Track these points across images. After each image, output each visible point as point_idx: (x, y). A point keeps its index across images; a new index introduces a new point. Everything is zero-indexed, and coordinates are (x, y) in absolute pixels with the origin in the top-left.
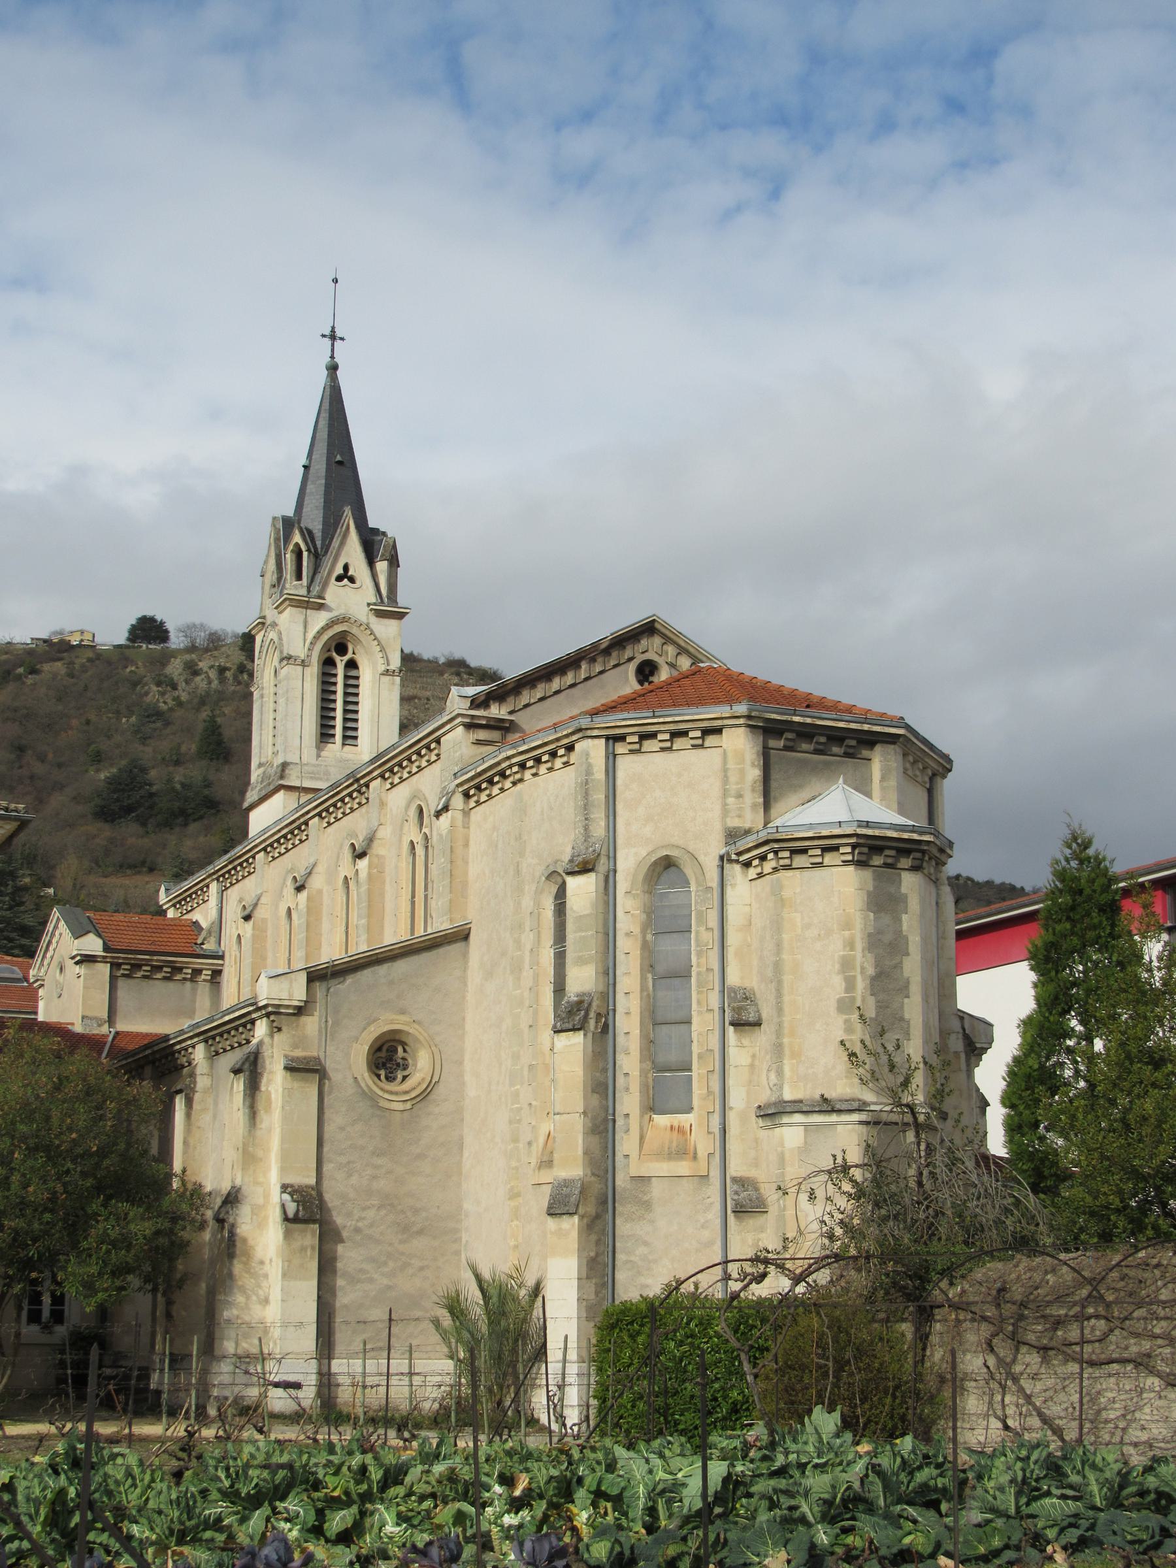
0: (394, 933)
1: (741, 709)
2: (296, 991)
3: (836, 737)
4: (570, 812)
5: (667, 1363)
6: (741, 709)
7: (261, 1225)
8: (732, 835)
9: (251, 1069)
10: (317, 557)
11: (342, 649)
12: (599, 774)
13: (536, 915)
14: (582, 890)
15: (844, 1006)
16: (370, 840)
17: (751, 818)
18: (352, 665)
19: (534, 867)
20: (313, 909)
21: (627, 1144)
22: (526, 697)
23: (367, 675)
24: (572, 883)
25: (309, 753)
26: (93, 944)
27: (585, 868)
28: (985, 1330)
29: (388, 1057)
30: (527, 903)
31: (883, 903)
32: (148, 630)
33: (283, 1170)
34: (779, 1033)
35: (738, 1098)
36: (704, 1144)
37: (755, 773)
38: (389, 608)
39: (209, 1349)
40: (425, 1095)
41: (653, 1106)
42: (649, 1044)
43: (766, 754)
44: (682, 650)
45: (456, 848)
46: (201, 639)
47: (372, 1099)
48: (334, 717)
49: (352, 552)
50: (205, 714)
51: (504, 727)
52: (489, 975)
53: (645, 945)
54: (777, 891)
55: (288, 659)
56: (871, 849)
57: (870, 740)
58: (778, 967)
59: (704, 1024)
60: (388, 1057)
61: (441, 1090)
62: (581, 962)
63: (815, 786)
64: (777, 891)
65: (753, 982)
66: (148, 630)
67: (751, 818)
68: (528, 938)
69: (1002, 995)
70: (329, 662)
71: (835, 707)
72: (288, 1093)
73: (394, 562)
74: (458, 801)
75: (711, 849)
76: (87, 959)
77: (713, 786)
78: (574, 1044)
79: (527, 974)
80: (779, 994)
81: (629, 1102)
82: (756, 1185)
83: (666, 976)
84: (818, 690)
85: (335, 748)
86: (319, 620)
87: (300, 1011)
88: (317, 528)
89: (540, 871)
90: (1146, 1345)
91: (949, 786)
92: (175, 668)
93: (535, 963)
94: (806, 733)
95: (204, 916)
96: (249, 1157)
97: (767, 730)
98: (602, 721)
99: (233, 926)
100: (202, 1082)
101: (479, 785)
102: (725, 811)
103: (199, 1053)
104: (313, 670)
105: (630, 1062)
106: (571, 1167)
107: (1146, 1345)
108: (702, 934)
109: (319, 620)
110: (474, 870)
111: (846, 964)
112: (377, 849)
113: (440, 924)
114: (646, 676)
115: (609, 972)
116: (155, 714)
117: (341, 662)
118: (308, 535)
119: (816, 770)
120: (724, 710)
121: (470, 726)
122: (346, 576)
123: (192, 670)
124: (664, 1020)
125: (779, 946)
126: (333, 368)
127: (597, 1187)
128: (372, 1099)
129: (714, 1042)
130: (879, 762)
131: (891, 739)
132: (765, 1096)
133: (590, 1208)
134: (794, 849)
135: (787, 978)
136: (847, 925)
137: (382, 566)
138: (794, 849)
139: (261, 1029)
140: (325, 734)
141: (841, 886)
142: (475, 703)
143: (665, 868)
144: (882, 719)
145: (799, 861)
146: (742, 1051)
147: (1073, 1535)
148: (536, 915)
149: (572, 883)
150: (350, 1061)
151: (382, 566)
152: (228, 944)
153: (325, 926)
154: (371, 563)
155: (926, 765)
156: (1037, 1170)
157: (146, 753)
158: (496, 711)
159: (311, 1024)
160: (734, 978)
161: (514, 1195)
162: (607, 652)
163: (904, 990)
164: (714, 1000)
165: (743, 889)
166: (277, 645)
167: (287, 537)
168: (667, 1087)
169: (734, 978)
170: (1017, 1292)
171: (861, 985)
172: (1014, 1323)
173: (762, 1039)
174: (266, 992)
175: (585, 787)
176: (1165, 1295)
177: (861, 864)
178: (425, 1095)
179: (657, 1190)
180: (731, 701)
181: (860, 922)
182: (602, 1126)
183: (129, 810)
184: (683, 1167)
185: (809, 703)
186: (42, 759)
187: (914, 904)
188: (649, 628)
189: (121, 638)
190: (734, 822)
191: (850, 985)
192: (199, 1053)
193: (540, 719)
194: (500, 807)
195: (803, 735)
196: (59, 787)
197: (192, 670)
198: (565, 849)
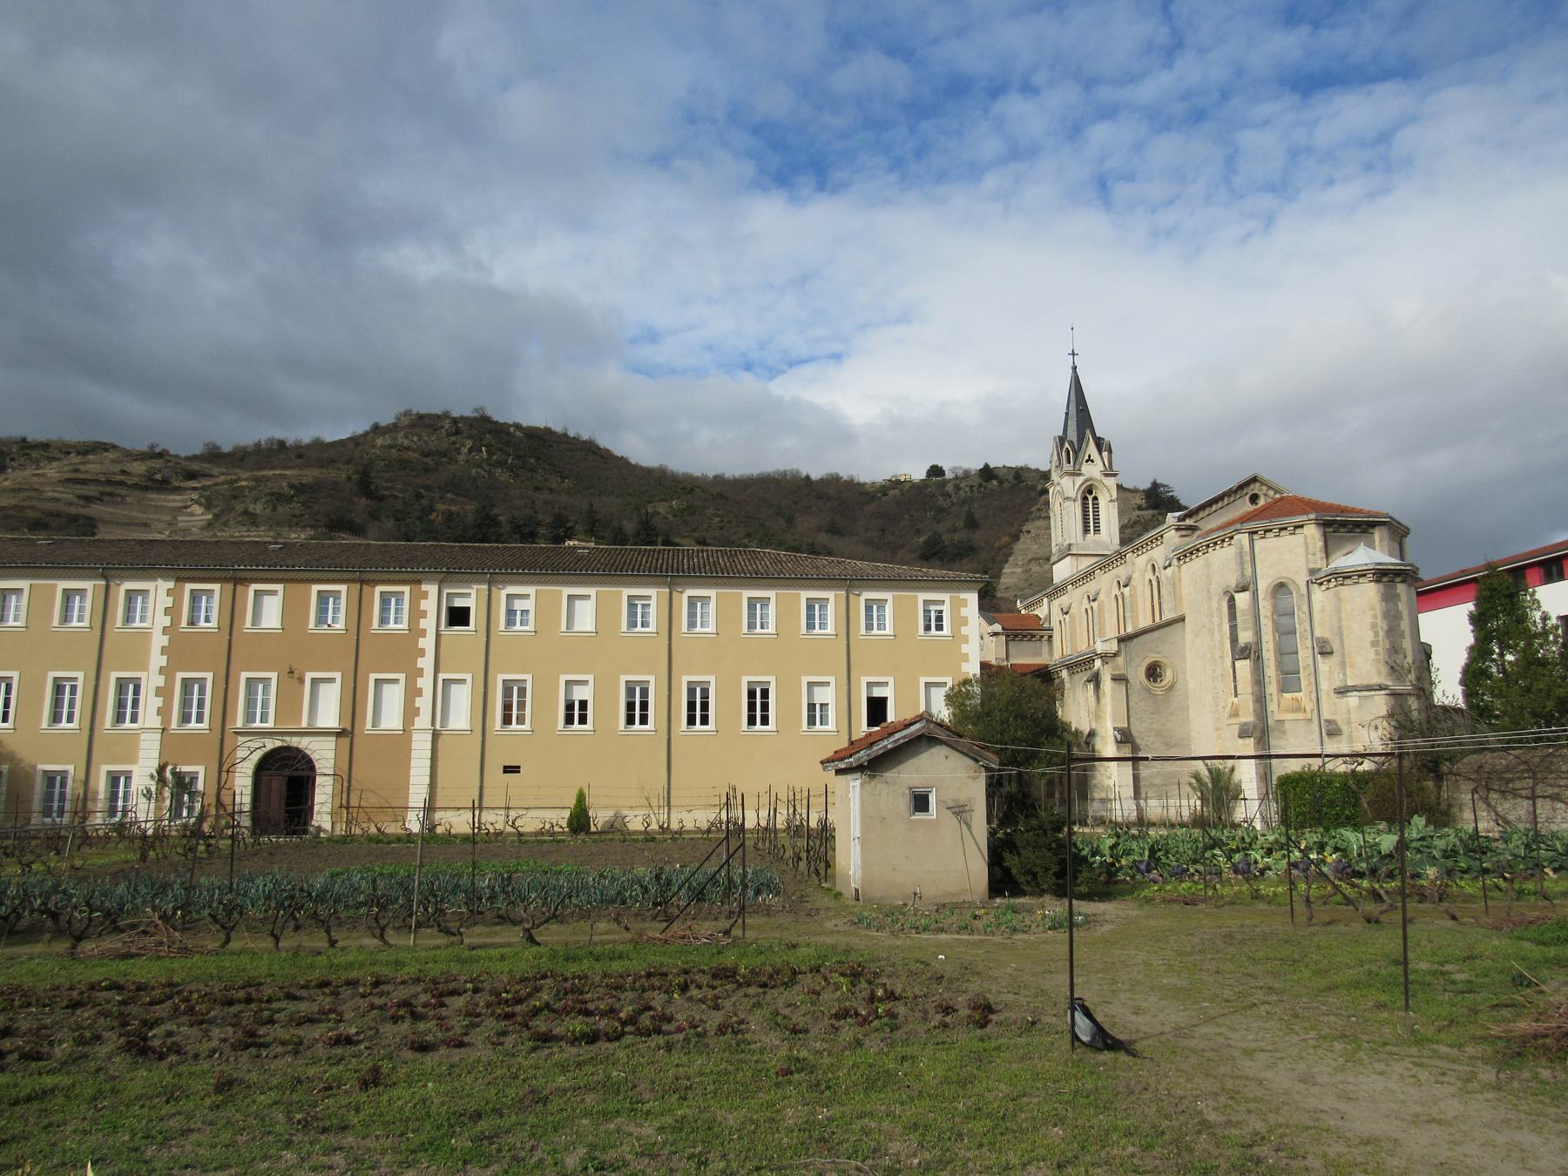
0: (1145, 622)
1: (1312, 516)
2: (1114, 647)
3: (1357, 524)
4: (1234, 565)
5: (1311, 800)
6: (1312, 516)
7: (1105, 744)
8: (1312, 572)
9: (1096, 679)
10: (1076, 453)
11: (1090, 492)
12: (1247, 548)
13: (1219, 609)
14: (1242, 599)
15: (1374, 644)
16: (1129, 579)
17: (1319, 562)
18: (1095, 498)
19: (1216, 589)
20: (1101, 608)
21: (1272, 706)
22: (1201, 515)
23: (1102, 502)
24: (1237, 596)
25: (1080, 539)
26: (997, 628)
27: (1244, 589)
28: (1471, 786)
29: (1153, 672)
30: (1214, 605)
31: (1389, 598)
32: (935, 471)
33: (1114, 721)
34: (1343, 655)
35: (1324, 685)
36: (1309, 705)
37: (1320, 544)
38: (1109, 472)
39: (1084, 796)
40: (1171, 688)
41: (1283, 689)
42: (1279, 664)
43: (1325, 535)
44: (1270, 488)
45: (1175, 583)
46: (960, 473)
47: (1149, 690)
48: (1089, 522)
49: (1092, 449)
50: (966, 508)
51: (1193, 529)
52: (1197, 635)
53: (1274, 621)
54: (1337, 595)
55: (1068, 498)
56: (1382, 575)
57: (1373, 525)
58: (1340, 628)
59: (1304, 655)
60: (1153, 672)
61: (1178, 686)
62: (1245, 629)
63: (1348, 548)
64: (1337, 595)
65: (1327, 635)
66: (935, 471)
67: (1319, 562)
68: (1216, 620)
69: (1449, 633)
70: (1085, 498)
71: (1353, 511)
72: (1113, 690)
73: (1110, 452)
74: (1175, 562)
75: (1302, 579)
76: (996, 634)
77: (1301, 550)
78: (1244, 666)
79: (1217, 636)
80: (1342, 640)
81: (1272, 688)
82: (1347, 724)
83: (1285, 632)
84: (1343, 503)
85: (1091, 535)
86: (1080, 480)
87: (1115, 655)
88: (1075, 440)
89: (1220, 590)
90: (1556, 790)
91: (1408, 541)
92: (949, 488)
93: (1220, 631)
94: (1343, 524)
95: (1041, 612)
96: (1098, 717)
97: (1325, 525)
98: (1246, 526)
99: (1057, 616)
100: (1067, 685)
101: (1185, 555)
102: (1308, 562)
103: (1065, 674)
104: (1079, 502)
105: (1271, 671)
106: (1248, 716)
107: (1556, 790)
108: (1301, 616)
109: (1080, 480)
110: (1185, 591)
111: (1374, 626)
112: (1133, 582)
113: (1168, 615)
114: (1260, 504)
115: (1258, 633)
116: (941, 510)
117: (1090, 498)
118: (1071, 443)
119: (1348, 540)
120: (1305, 517)
121: (1178, 529)
122: (1089, 460)
123: (957, 488)
124: (1286, 653)
125: (1340, 619)
126: (1075, 368)
127: (1260, 725)
128: (1149, 690)
129: (1310, 661)
130: (1378, 535)
131: (1383, 523)
132: (1338, 684)
133: (1258, 734)
134: (1343, 577)
135: (1345, 633)
136: (1373, 609)
137: (1105, 454)
138: (1343, 577)
139: (1098, 663)
140: (1086, 530)
141: (1369, 592)
142: (1181, 519)
143: (1280, 587)
144: (1377, 515)
145: (1347, 581)
146: (1324, 665)
147: (1556, 865)
148: (1219, 609)
149: (1237, 596)
150: (1138, 674)
151: (1105, 454)
152: (1055, 624)
153: (1107, 616)
154: (1100, 452)
155: (1398, 532)
156: (1477, 711)
157: (940, 528)
158: (1188, 522)
159: (1120, 660)
160: (1318, 633)
161: (1217, 729)
162: (1236, 492)
163: (1402, 635)
164: (1309, 644)
165: (1318, 594)
166: (1061, 493)
167: (1062, 445)
168: (1289, 681)
169: (1318, 633)
170: (1487, 768)
171: (1381, 634)
172: (1489, 783)
173: (1335, 659)
174: (1100, 647)
175: (1240, 555)
176: (1564, 768)
177: (1377, 581)
178: (1171, 688)
179: (1288, 726)
180: (1306, 513)
181: (1379, 608)
182: (1261, 700)
183: (934, 555)
184: (1300, 716)
185: (1344, 510)
186: (893, 534)
187: (1404, 597)
188: (1254, 480)
189: (923, 476)
190: (1312, 566)
191: (1376, 634)
192: (1065, 674)
193: (1210, 522)
194: (1196, 565)
195: (1342, 526)
196: (902, 546)
197: (957, 488)
198: (1233, 583)
